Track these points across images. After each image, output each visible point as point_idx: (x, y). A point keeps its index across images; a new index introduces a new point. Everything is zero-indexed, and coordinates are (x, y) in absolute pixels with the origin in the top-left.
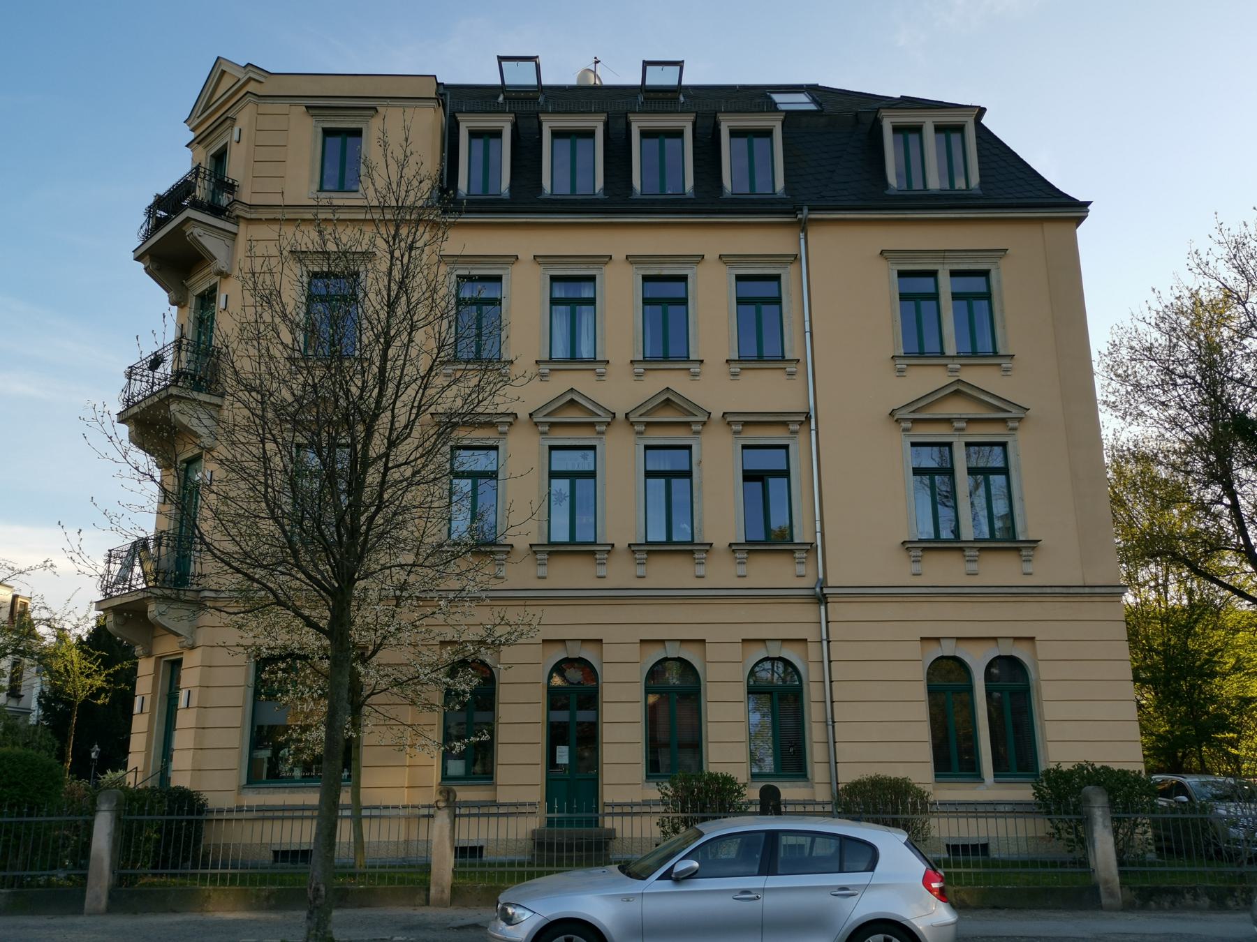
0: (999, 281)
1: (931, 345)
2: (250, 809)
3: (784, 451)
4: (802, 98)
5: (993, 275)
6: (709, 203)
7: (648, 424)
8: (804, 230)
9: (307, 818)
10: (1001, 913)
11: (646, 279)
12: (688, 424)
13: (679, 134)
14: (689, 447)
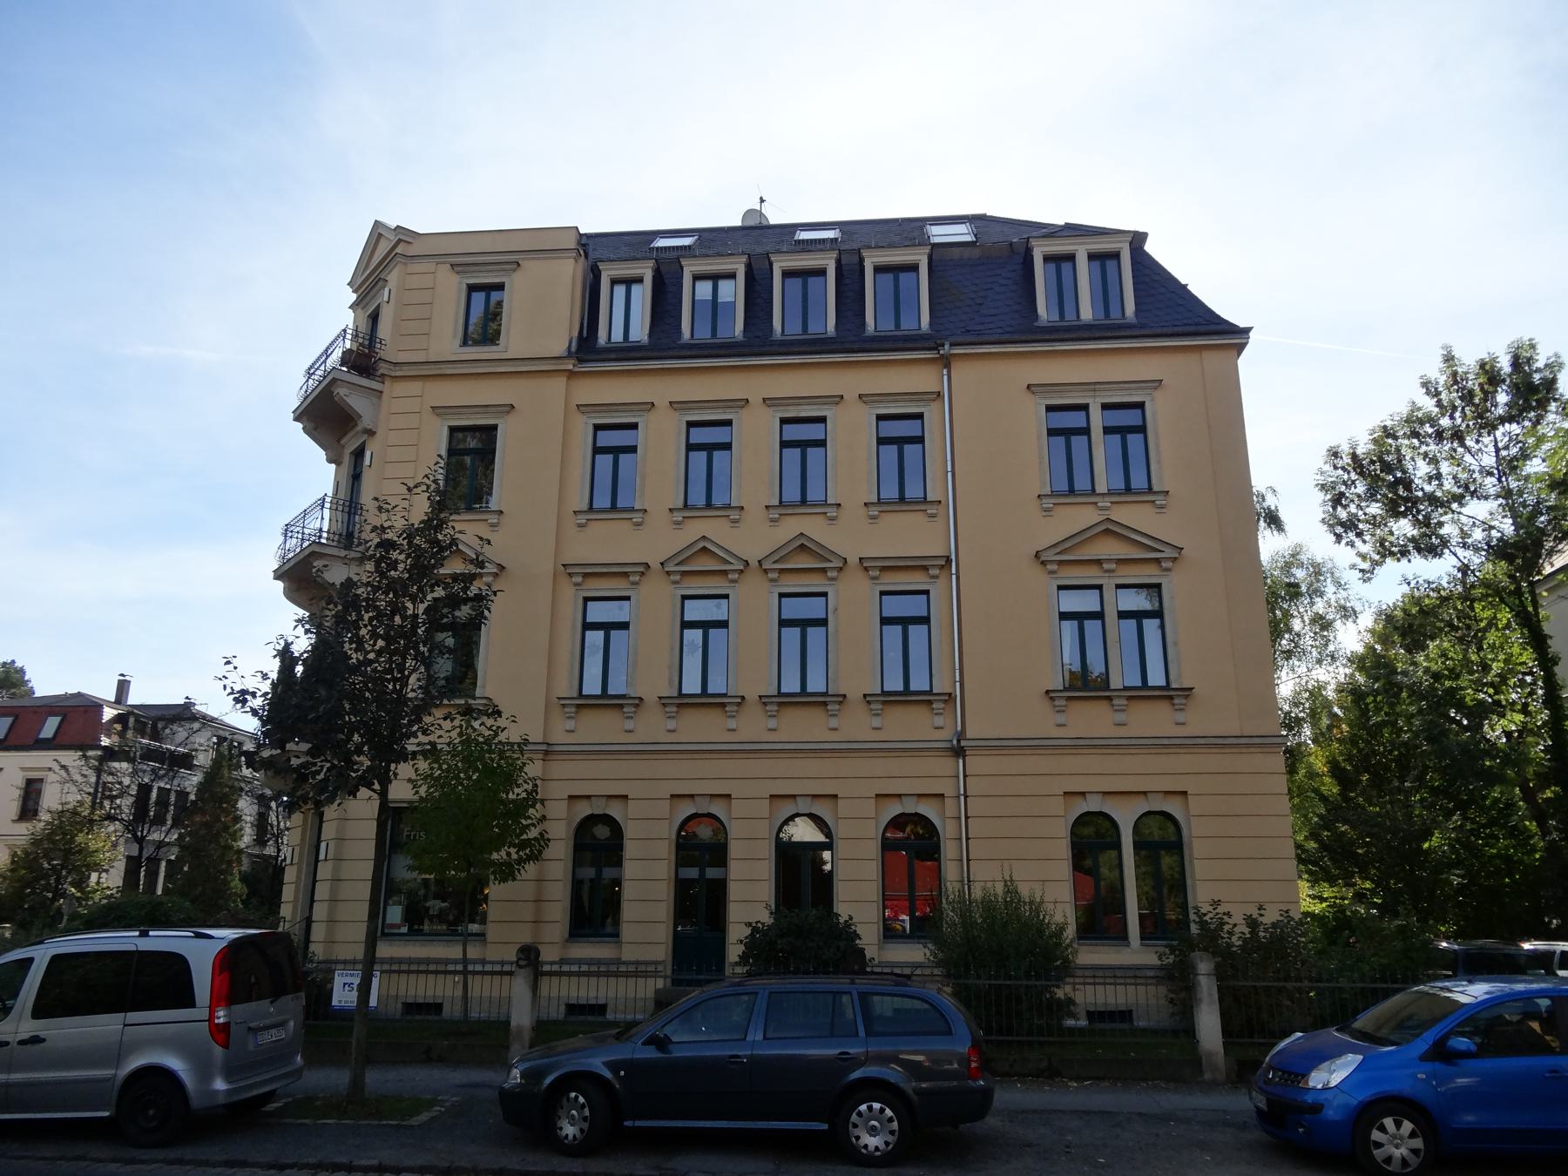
1: (1081, 483)
2: (580, 962)
5: (1148, 406)
7: (782, 571)
8: (948, 366)
9: (450, 972)
12: (824, 570)
13: (914, 268)
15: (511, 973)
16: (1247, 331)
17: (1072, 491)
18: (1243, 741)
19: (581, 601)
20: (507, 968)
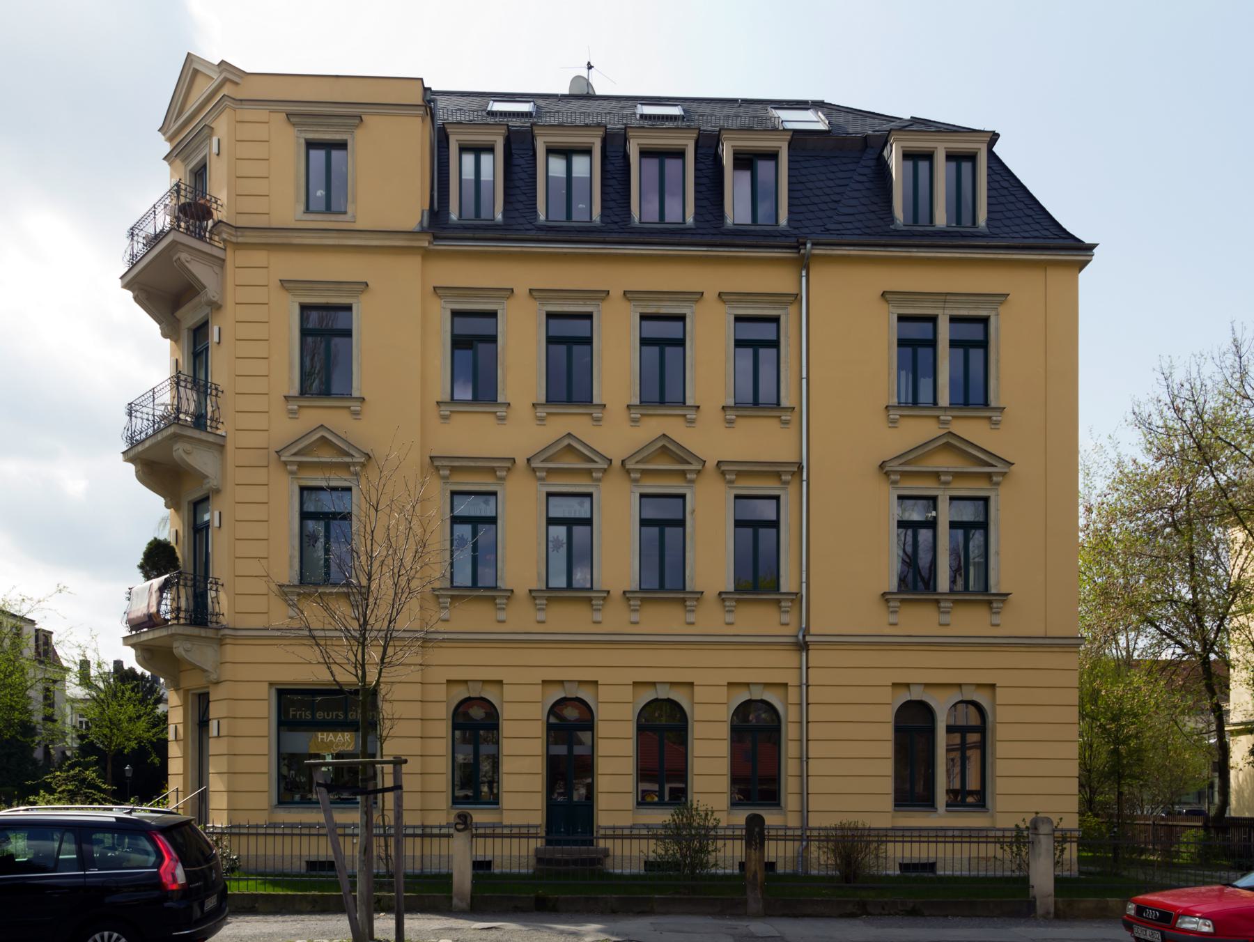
0: (997, 329)
3: (774, 501)
4: (809, 115)
5: (992, 321)
6: (710, 232)
10: (857, 922)
11: (643, 317)
14: (683, 497)
15: (449, 836)
16: (1091, 247)
17: (756, 403)
18: (1047, 641)
19: (448, 494)
20: (444, 831)
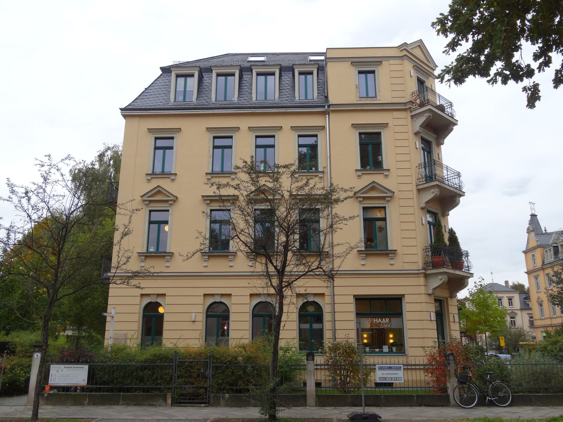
19: (148, 212)
